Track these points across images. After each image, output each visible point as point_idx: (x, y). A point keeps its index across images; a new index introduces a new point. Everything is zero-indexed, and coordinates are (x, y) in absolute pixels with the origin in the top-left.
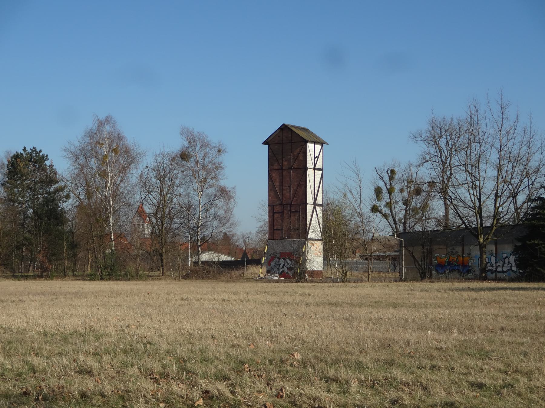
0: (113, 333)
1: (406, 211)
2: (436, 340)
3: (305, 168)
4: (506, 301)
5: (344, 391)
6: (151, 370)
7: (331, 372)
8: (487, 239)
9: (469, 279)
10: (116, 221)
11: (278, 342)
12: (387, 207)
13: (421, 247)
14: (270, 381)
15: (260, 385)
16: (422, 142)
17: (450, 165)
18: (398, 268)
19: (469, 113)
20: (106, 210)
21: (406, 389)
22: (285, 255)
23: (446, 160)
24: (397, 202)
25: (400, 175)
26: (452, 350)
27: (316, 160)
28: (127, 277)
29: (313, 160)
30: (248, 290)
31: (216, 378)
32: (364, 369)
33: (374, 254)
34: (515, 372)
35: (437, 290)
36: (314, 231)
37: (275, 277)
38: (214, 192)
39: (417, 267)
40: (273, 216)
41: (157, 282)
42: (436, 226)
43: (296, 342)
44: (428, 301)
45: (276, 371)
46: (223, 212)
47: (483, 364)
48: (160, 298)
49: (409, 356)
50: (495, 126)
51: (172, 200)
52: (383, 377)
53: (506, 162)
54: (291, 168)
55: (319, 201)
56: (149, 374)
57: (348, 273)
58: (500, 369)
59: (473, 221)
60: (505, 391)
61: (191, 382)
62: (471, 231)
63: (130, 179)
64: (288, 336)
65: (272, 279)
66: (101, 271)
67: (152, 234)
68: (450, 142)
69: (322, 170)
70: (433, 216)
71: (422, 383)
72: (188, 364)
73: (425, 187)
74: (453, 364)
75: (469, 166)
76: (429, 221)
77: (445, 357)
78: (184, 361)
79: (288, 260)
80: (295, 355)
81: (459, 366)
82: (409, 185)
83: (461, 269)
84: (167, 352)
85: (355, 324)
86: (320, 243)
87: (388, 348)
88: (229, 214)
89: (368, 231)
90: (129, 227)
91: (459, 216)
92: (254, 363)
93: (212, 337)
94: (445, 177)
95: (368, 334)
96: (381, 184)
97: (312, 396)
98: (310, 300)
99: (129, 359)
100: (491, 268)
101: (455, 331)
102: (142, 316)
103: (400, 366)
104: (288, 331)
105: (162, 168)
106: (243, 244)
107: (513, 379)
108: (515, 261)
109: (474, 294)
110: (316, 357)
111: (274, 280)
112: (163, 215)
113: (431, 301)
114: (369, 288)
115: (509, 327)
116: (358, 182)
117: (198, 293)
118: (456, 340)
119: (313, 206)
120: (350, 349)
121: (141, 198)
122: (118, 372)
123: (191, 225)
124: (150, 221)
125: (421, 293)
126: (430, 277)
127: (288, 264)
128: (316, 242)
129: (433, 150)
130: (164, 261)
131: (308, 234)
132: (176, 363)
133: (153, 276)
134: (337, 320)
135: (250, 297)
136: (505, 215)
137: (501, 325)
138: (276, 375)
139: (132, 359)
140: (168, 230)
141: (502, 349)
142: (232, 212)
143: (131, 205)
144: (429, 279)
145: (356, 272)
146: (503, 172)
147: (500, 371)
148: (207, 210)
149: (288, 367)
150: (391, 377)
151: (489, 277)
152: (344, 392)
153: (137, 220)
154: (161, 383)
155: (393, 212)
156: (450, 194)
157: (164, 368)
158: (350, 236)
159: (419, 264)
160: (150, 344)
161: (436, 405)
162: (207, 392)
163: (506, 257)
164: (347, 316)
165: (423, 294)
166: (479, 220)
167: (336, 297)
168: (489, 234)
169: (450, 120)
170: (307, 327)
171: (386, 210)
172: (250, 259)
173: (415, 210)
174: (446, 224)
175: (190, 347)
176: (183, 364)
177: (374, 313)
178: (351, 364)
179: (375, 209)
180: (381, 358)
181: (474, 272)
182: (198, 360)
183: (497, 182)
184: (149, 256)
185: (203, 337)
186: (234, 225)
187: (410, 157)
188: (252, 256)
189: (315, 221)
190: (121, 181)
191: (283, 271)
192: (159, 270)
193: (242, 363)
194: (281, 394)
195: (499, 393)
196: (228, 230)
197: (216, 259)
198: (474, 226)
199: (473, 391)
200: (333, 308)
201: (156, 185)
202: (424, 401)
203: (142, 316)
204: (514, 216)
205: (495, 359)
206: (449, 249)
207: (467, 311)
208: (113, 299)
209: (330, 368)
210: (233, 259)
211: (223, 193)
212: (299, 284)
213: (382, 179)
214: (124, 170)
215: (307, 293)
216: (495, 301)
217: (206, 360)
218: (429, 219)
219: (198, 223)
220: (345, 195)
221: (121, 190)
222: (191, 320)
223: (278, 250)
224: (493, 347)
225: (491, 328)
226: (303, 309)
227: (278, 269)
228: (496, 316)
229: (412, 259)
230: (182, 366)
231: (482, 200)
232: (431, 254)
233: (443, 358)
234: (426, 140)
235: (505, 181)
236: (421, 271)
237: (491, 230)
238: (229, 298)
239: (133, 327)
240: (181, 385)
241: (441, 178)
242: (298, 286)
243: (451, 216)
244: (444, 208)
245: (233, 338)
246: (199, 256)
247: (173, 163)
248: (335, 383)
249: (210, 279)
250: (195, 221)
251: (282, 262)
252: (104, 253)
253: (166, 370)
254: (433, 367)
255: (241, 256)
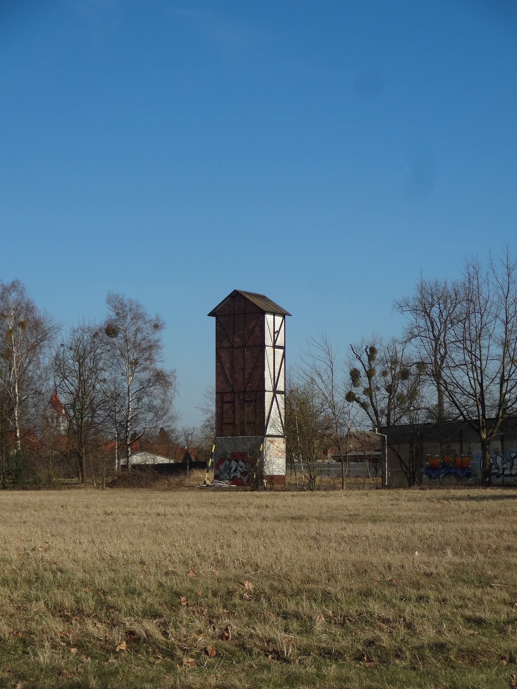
0: (15, 557)
2: (424, 563)
3: (263, 346)
5: (307, 630)
6: (62, 605)
7: (291, 606)
8: (492, 434)
9: (469, 485)
10: (22, 414)
12: (366, 395)
14: (213, 618)
15: (199, 624)
16: (409, 312)
18: (380, 472)
19: (467, 275)
20: (10, 399)
21: (384, 626)
22: (237, 456)
23: (440, 335)
24: (378, 389)
25: (382, 354)
26: (444, 576)
27: (276, 335)
28: (36, 485)
29: (272, 336)
30: (189, 502)
32: (333, 601)
33: (350, 454)
35: (429, 500)
36: (273, 426)
37: (224, 484)
39: (404, 470)
40: (222, 406)
41: (74, 491)
42: (428, 417)
44: (417, 513)
46: (160, 401)
48: (77, 513)
49: (390, 584)
50: (500, 292)
52: (357, 611)
54: (244, 346)
55: (281, 387)
56: (58, 611)
57: (318, 479)
58: (504, 599)
59: (473, 410)
60: (510, 628)
61: (112, 620)
63: (41, 360)
64: (238, 560)
65: (221, 486)
66: (4, 477)
67: (69, 429)
68: (445, 313)
69: (283, 348)
70: (423, 406)
72: (109, 598)
73: (414, 369)
74: (445, 594)
75: (468, 342)
76: (419, 412)
77: (436, 585)
78: (104, 593)
79: (241, 463)
80: (246, 585)
81: (452, 597)
83: (460, 473)
85: (324, 543)
86: (281, 440)
87: (364, 574)
88: (167, 405)
89: (342, 425)
90: (39, 421)
91: (456, 405)
93: (141, 563)
94: (439, 356)
95: (340, 557)
96: (358, 366)
97: (266, 637)
98: (268, 513)
99: (33, 592)
100: (496, 471)
101: (449, 551)
102: (53, 535)
103: (379, 597)
105: (81, 346)
109: (474, 504)
110: (272, 587)
111: (224, 488)
112: (83, 405)
114: (344, 498)
116: (329, 363)
118: (451, 563)
119: (272, 393)
121: (55, 384)
122: (18, 608)
123: (118, 418)
125: (408, 504)
127: (241, 467)
128: (276, 439)
129: (422, 323)
130: (84, 465)
132: (93, 596)
133: (70, 484)
135: (192, 510)
137: (507, 543)
138: (221, 610)
139: (37, 591)
140: (90, 425)
141: (508, 574)
142: (171, 402)
144: (419, 485)
146: (510, 350)
147: (504, 602)
148: (139, 399)
149: (237, 600)
150: (367, 612)
151: (494, 482)
153: (50, 412)
154: (74, 621)
156: (444, 378)
158: (320, 431)
159: (406, 466)
160: (61, 571)
162: (131, 633)
164: (313, 534)
165: (411, 504)
166: (481, 411)
167: (301, 509)
168: (494, 428)
169: (443, 285)
170: (262, 548)
171: (364, 398)
173: (401, 398)
174: (440, 415)
175: (112, 575)
176: (103, 597)
177: (348, 530)
179: (350, 397)
180: (354, 587)
181: (476, 475)
182: (122, 592)
183: (503, 363)
185: (130, 562)
186: (173, 418)
187: (393, 330)
188: (196, 457)
189: (275, 411)
190: (29, 363)
192: (78, 476)
193: (178, 595)
194: (227, 634)
195: (502, 631)
196: (166, 424)
197: (150, 462)
198: (475, 418)
199: (470, 628)
200: (296, 524)
201: (73, 368)
202: (407, 642)
203: (53, 535)
205: (498, 587)
207: (464, 526)
208: (17, 513)
209: (289, 601)
210: (172, 461)
212: (255, 493)
213: (360, 359)
214: (33, 349)
215: (264, 505)
216: (500, 512)
217: (131, 592)
218: (419, 409)
219: (128, 416)
220: (312, 379)
221: (30, 374)
222: (115, 541)
224: (496, 572)
225: (494, 547)
226: (257, 524)
227: (229, 474)
228: (501, 532)
230: (100, 600)
231: (484, 384)
236: (408, 475)
240: (99, 625)
241: (433, 358)
242: (253, 495)
243: (446, 405)
244: (437, 395)
245: (167, 563)
246: (128, 457)
247: (95, 340)
248: (295, 619)
249: (143, 487)
250: (124, 413)
251: (234, 464)
252: (7, 454)
253: (80, 605)
254: (420, 598)
255: (182, 457)
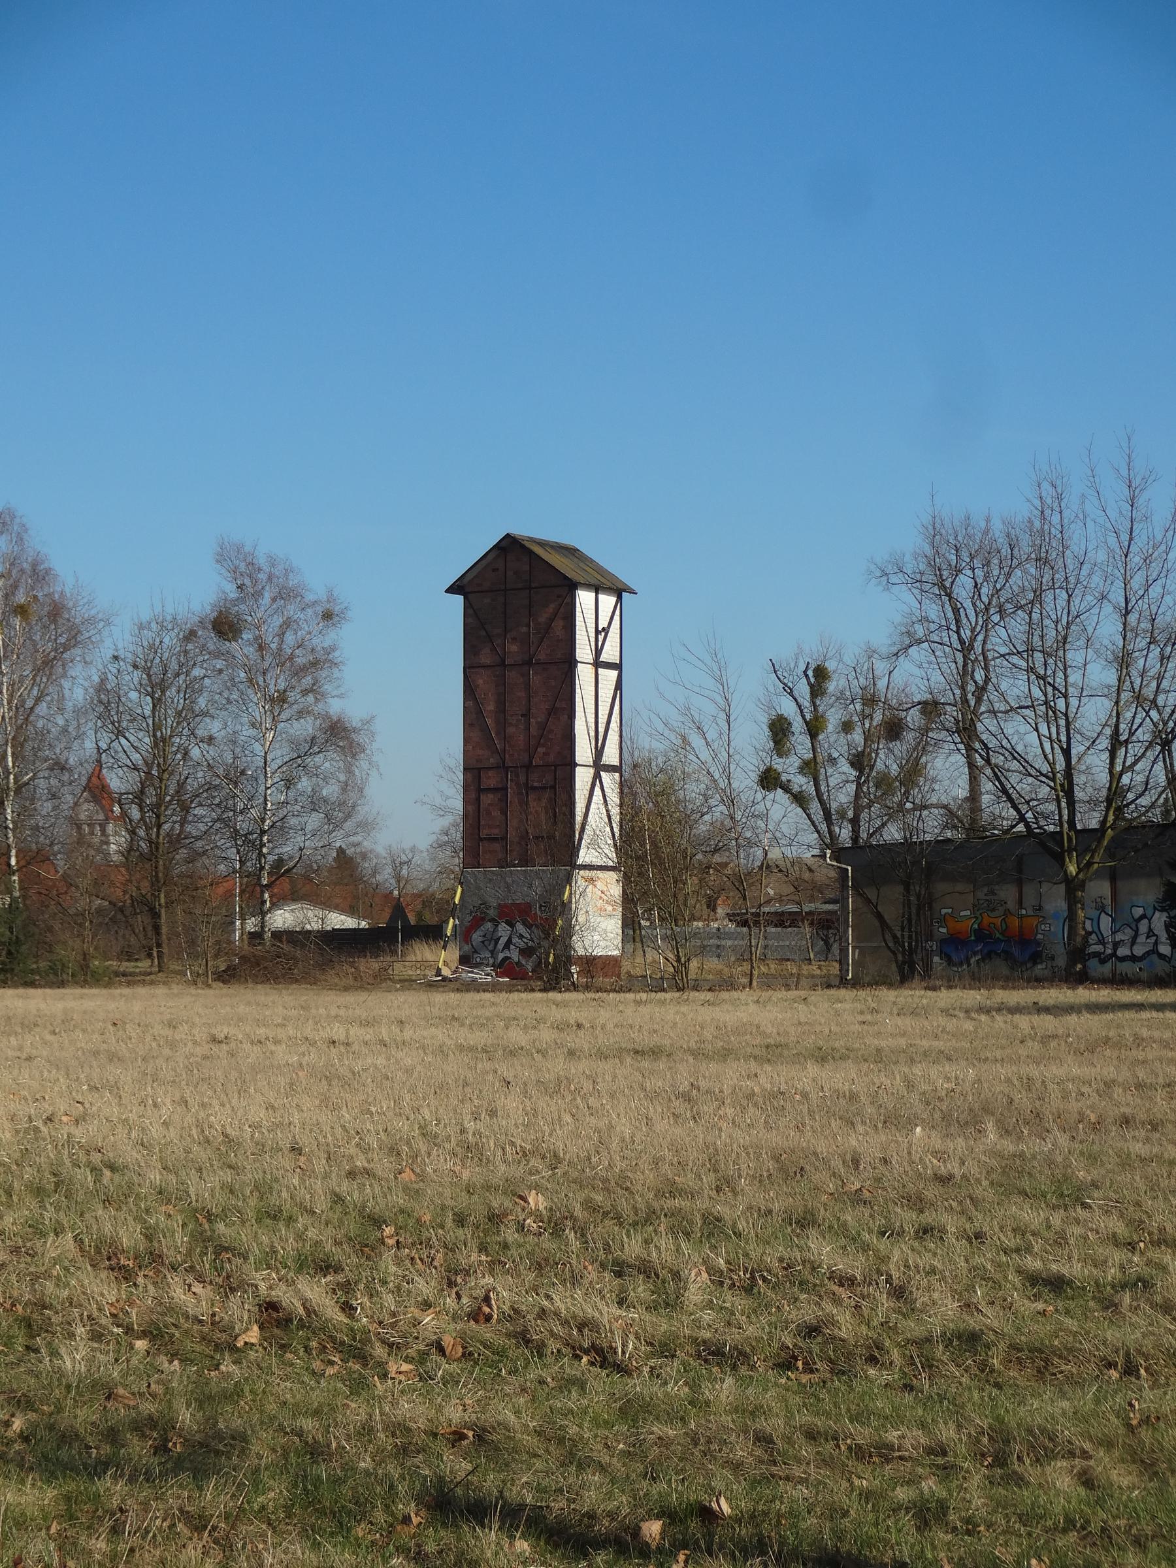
1: (859, 786)
2: (935, 1153)
4: (1139, 1041)
5: (668, 1301)
6: (114, 1243)
7: (632, 1248)
8: (1089, 864)
9: (1038, 980)
10: (23, 813)
11: (483, 1161)
12: (805, 775)
13: (900, 889)
15: (424, 1287)
16: (904, 587)
17: (983, 654)
18: (835, 948)
19: (1037, 503)
21: (843, 1293)
22: (511, 913)
23: (973, 639)
24: (832, 761)
25: (843, 682)
26: (978, 1181)
27: (601, 638)
28: (56, 977)
29: (593, 640)
30: (403, 1015)
31: (301, 1267)
33: (767, 910)
34: (1158, 1243)
35: (946, 1012)
37: (480, 975)
38: (311, 731)
39: (891, 944)
40: (478, 799)
41: (141, 991)
42: (945, 827)
43: (536, 1162)
44: (918, 1042)
45: (474, 1244)
47: (1066, 1221)
48: (148, 1038)
49: (857, 1199)
50: (1112, 540)
51: (186, 753)
52: (781, 1260)
53: (1142, 643)
54: (529, 663)
55: (611, 756)
57: (694, 964)
58: (1114, 1235)
60: (1127, 1298)
61: (228, 1277)
62: (1042, 844)
64: (513, 1144)
65: (474, 980)
68: (986, 589)
69: (618, 667)
70: (934, 800)
71: (889, 1277)
72: (221, 1227)
73: (913, 717)
74: (981, 1222)
76: (925, 813)
78: (210, 1217)
79: (520, 928)
81: (997, 1229)
82: (867, 711)
83: (1015, 950)
84: (160, 1193)
85: (707, 1109)
86: (613, 876)
88: (353, 795)
89: (750, 843)
90: (62, 830)
91: (1010, 799)
92: (411, 1222)
93: (293, 1149)
94: (971, 688)
95: (743, 1138)
96: (788, 708)
97: (574, 1317)
98: (581, 1040)
99: (49, 1214)
102: (93, 1088)
104: (512, 1130)
105: (158, 660)
106: (393, 881)
107: (1149, 1262)
108: (1167, 927)
109: (1048, 1023)
110: (590, 1206)
113: (925, 1043)
114: (752, 1008)
115: (1142, 1116)
117: (259, 1023)
118: (993, 1153)
119: (592, 771)
120: (686, 1180)
121: (98, 748)
122: (15, 1250)
123: (242, 825)
124: (124, 814)
125: (899, 1021)
126: (927, 973)
127: (521, 937)
128: (600, 874)
129: (933, 611)
131: (578, 851)
132: (184, 1225)
133: (132, 974)
134: (653, 1096)
135: (408, 1033)
136: (1140, 796)
138: (474, 1256)
140: (176, 841)
141: (1124, 1178)
142: (361, 790)
143: (70, 770)
145: (715, 959)
147: (1115, 1240)
148: (289, 783)
149: (510, 1235)
150: (804, 1262)
151: (1092, 973)
152: (667, 1304)
153: (87, 810)
155: (823, 788)
156: (984, 737)
157: (149, 1238)
158: (699, 856)
159: (895, 937)
160: (113, 1168)
161: (928, 1340)
162: (272, 1306)
163: (1143, 917)
164: (684, 1087)
165: (906, 1022)
166: (1065, 812)
168: (1094, 852)
169: (983, 524)
170: (567, 1118)
171: (801, 782)
172: (413, 923)
173: (883, 781)
174: (973, 821)
175: (228, 1176)
176: (207, 1227)
177: (763, 1080)
178: (691, 1222)
179: (769, 780)
180: (776, 1206)
181: (1053, 958)
182: (251, 1214)
183: (1117, 703)
184: (120, 916)
185: (267, 1148)
186: (366, 826)
187: (869, 628)
188: (419, 915)
189: (597, 811)
190: (38, 700)
191: (506, 958)
192: (150, 956)
193: (377, 1222)
194: (487, 1310)
195: (1110, 1305)
196: (351, 839)
197: (314, 925)
198: (1051, 828)
199: (1037, 1297)
200: (646, 1064)
201: (139, 711)
202: (895, 1329)
203: (93, 1088)
204: (1166, 800)
205: (1100, 1207)
206: (981, 894)
208: (12, 1039)
209: (628, 1236)
210: (364, 924)
211: (337, 733)
212: (552, 995)
213: (791, 694)
215: (572, 1022)
216: (1107, 1040)
217: (272, 1215)
218: (925, 807)
219: (263, 820)
220: (684, 740)
221: (40, 724)
222: (235, 1101)
223: (493, 897)
224: (1095, 1174)
225: (1093, 1118)
226: (558, 1066)
227: (492, 952)
229: (877, 923)
231: (1074, 752)
232: (930, 908)
233: (954, 1204)
234: (917, 582)
235: (1138, 698)
236: (900, 957)
237: (1100, 840)
238: (347, 1037)
239: (65, 1119)
240: (197, 1288)
241: (957, 692)
242: (548, 1000)
243: (986, 799)
244: (966, 777)
245: (353, 1151)
246: (263, 914)
249: (297, 981)
251: (504, 931)
253: (156, 1244)
254: (925, 1231)
